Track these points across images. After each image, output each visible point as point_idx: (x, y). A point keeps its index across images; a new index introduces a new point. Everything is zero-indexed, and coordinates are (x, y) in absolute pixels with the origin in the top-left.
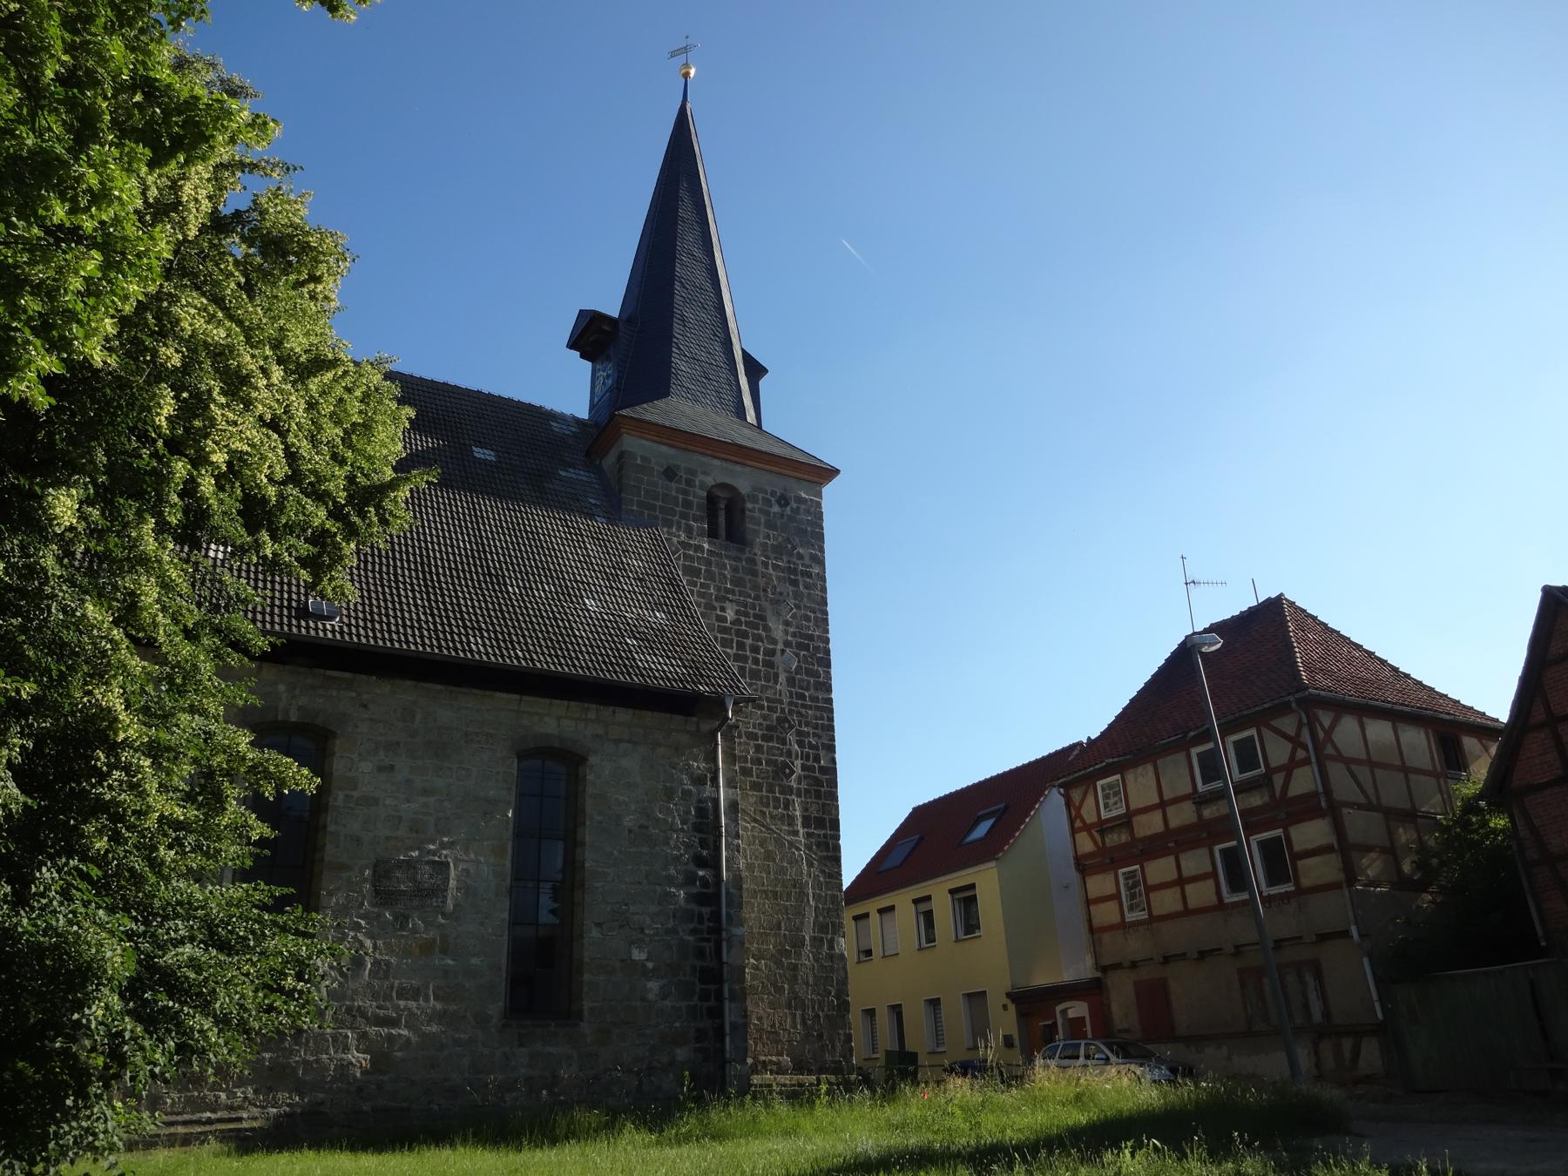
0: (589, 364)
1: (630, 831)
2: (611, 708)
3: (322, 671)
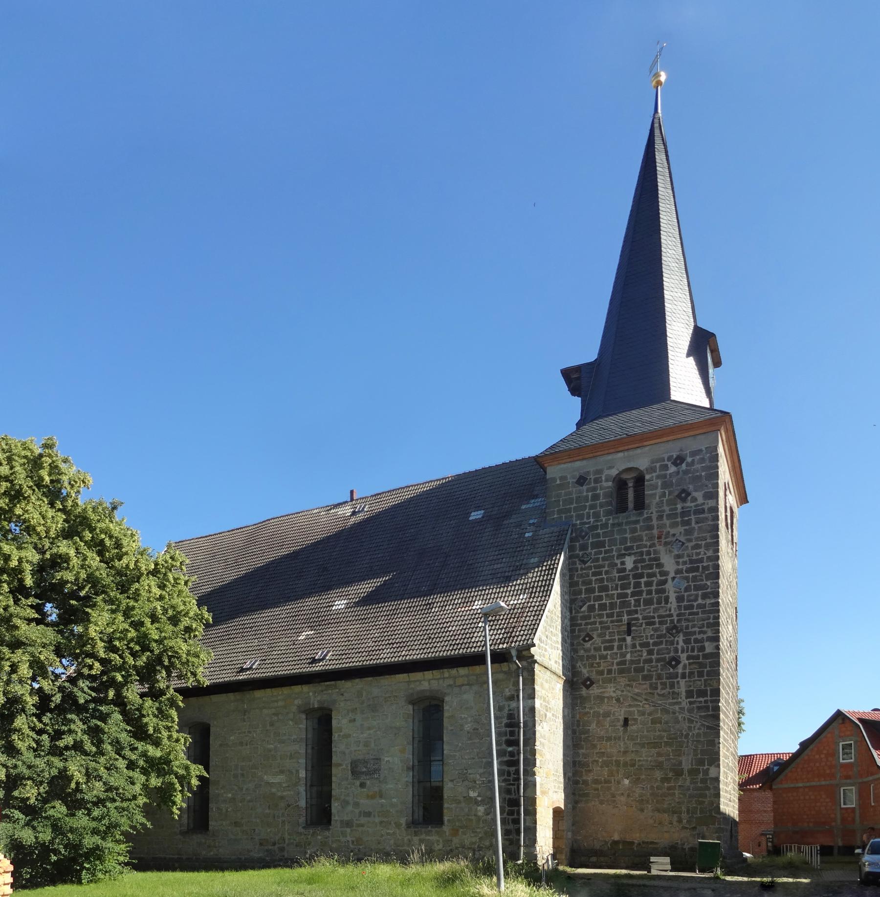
0: (577, 401)
1: (468, 732)
2: (455, 669)
3: (323, 683)
